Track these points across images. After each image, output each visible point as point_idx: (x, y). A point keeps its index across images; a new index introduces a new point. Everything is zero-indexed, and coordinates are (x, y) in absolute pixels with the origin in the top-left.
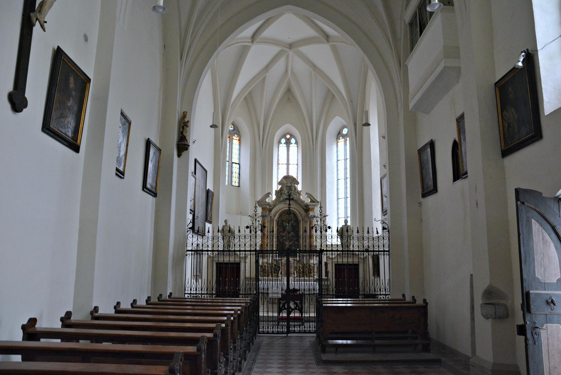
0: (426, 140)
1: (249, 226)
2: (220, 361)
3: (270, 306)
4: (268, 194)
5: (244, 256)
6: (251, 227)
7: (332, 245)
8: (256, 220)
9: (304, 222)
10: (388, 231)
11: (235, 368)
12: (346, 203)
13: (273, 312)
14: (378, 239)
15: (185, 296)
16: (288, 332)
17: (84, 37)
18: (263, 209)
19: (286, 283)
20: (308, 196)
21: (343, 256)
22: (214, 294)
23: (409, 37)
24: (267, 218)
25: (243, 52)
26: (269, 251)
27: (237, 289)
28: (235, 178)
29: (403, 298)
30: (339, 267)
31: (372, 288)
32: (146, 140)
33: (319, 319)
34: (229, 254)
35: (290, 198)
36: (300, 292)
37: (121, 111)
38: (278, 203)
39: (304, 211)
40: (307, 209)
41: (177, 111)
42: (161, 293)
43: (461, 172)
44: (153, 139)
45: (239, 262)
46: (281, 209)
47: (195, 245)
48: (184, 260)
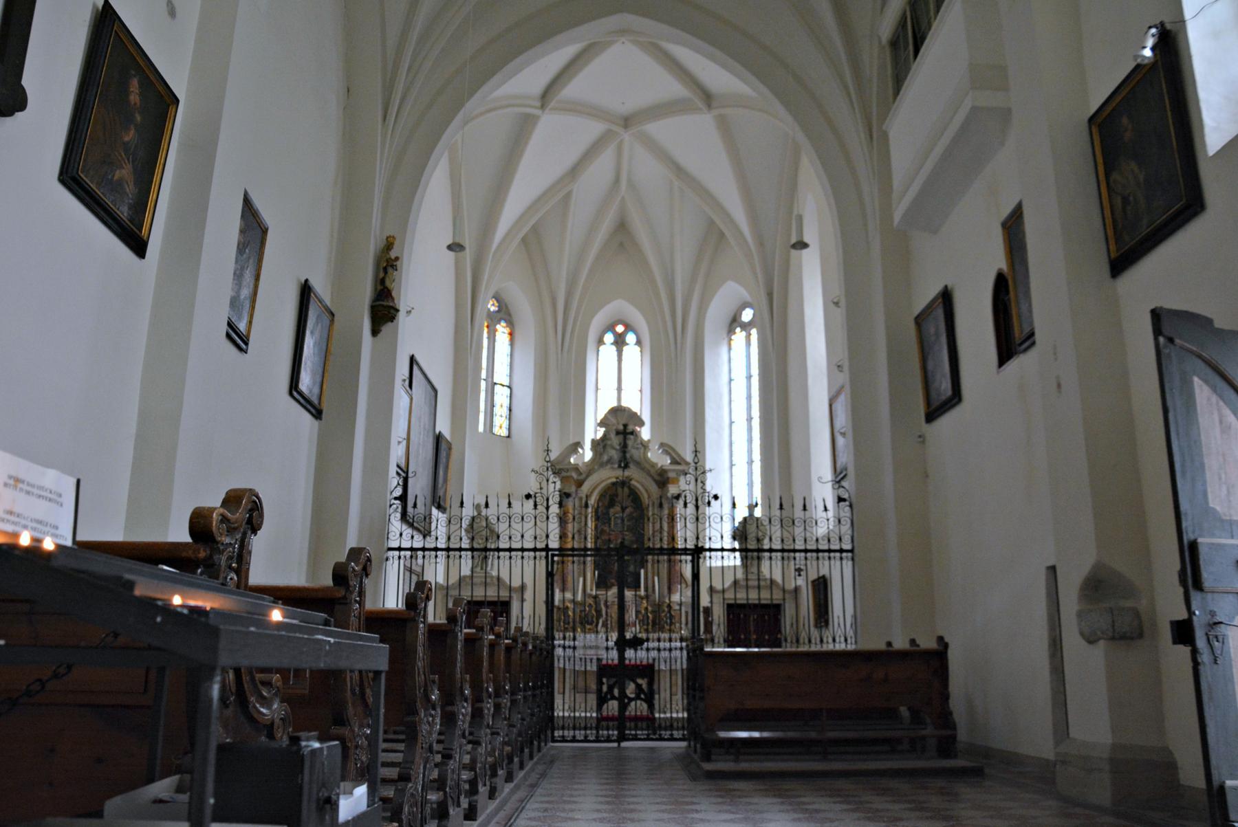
0: (934, 291)
1: (532, 493)
3: (580, 697)
4: (578, 445)
6: (537, 495)
10: (851, 506)
13: (586, 693)
17: (168, 5)
23: (889, 72)
25: (523, 128)
26: (576, 550)
35: (624, 463)
36: (648, 645)
38: (596, 467)
40: (662, 479)
41: (373, 232)
43: (1017, 334)
44: (320, 286)
45: (507, 599)
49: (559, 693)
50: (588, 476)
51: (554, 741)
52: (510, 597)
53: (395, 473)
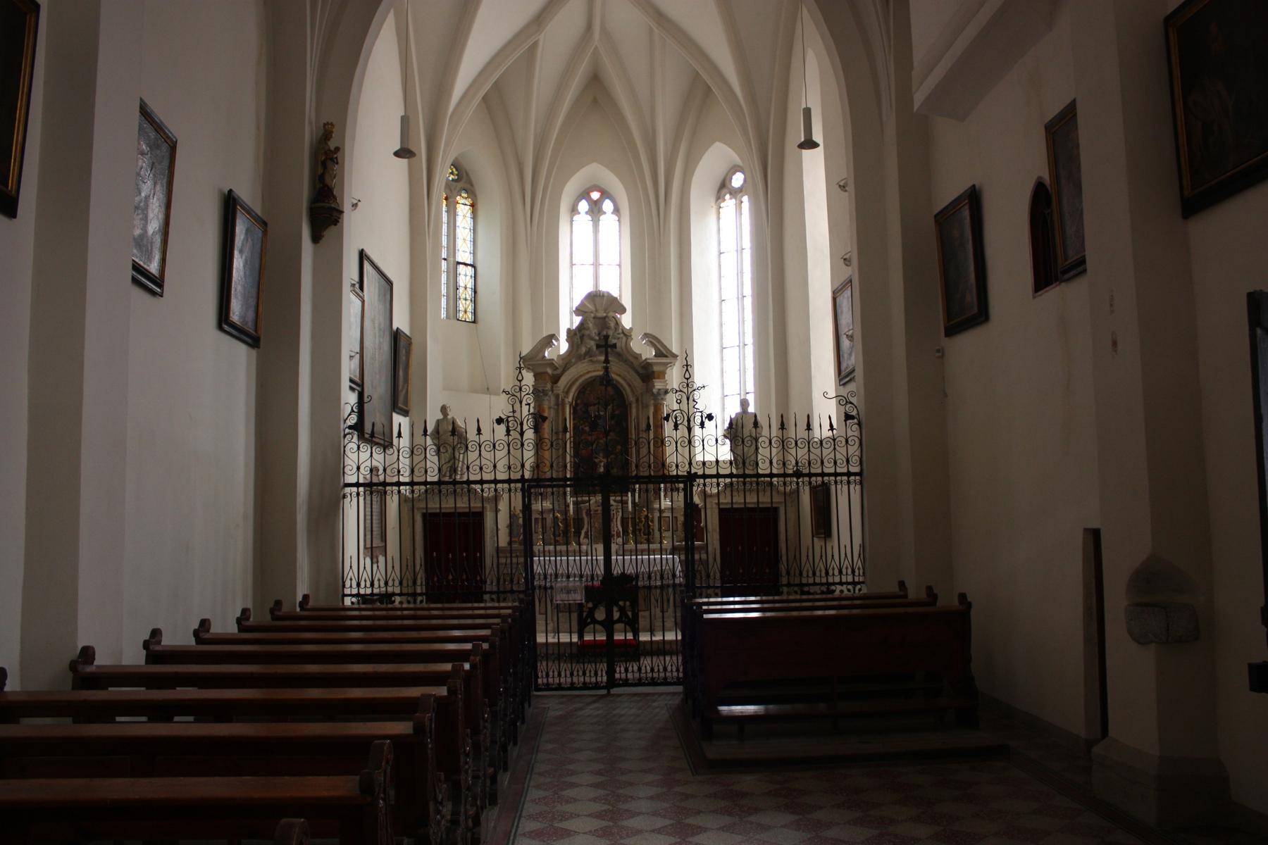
1: (503, 417)
2: (435, 798)
4: (550, 339)
5: (492, 494)
6: (510, 419)
7: (717, 461)
8: (521, 402)
9: (640, 407)
10: (859, 424)
11: (478, 803)
12: (742, 358)
14: (835, 445)
15: (343, 603)
16: (612, 683)
18: (537, 376)
19: (601, 558)
20: (651, 342)
21: (758, 489)
22: (421, 594)
24: (547, 397)
27: (478, 578)
28: (464, 302)
29: (900, 590)
30: (727, 516)
31: (807, 568)
32: (225, 195)
33: (687, 648)
34: (455, 491)
37: (141, 105)
38: (573, 360)
39: (639, 380)
42: (279, 598)
45: (481, 510)
46: (581, 376)
47: (365, 471)
48: (339, 509)
49: (540, 613)
50: (564, 371)
51: (538, 689)
52: (483, 507)
53: (348, 388)
